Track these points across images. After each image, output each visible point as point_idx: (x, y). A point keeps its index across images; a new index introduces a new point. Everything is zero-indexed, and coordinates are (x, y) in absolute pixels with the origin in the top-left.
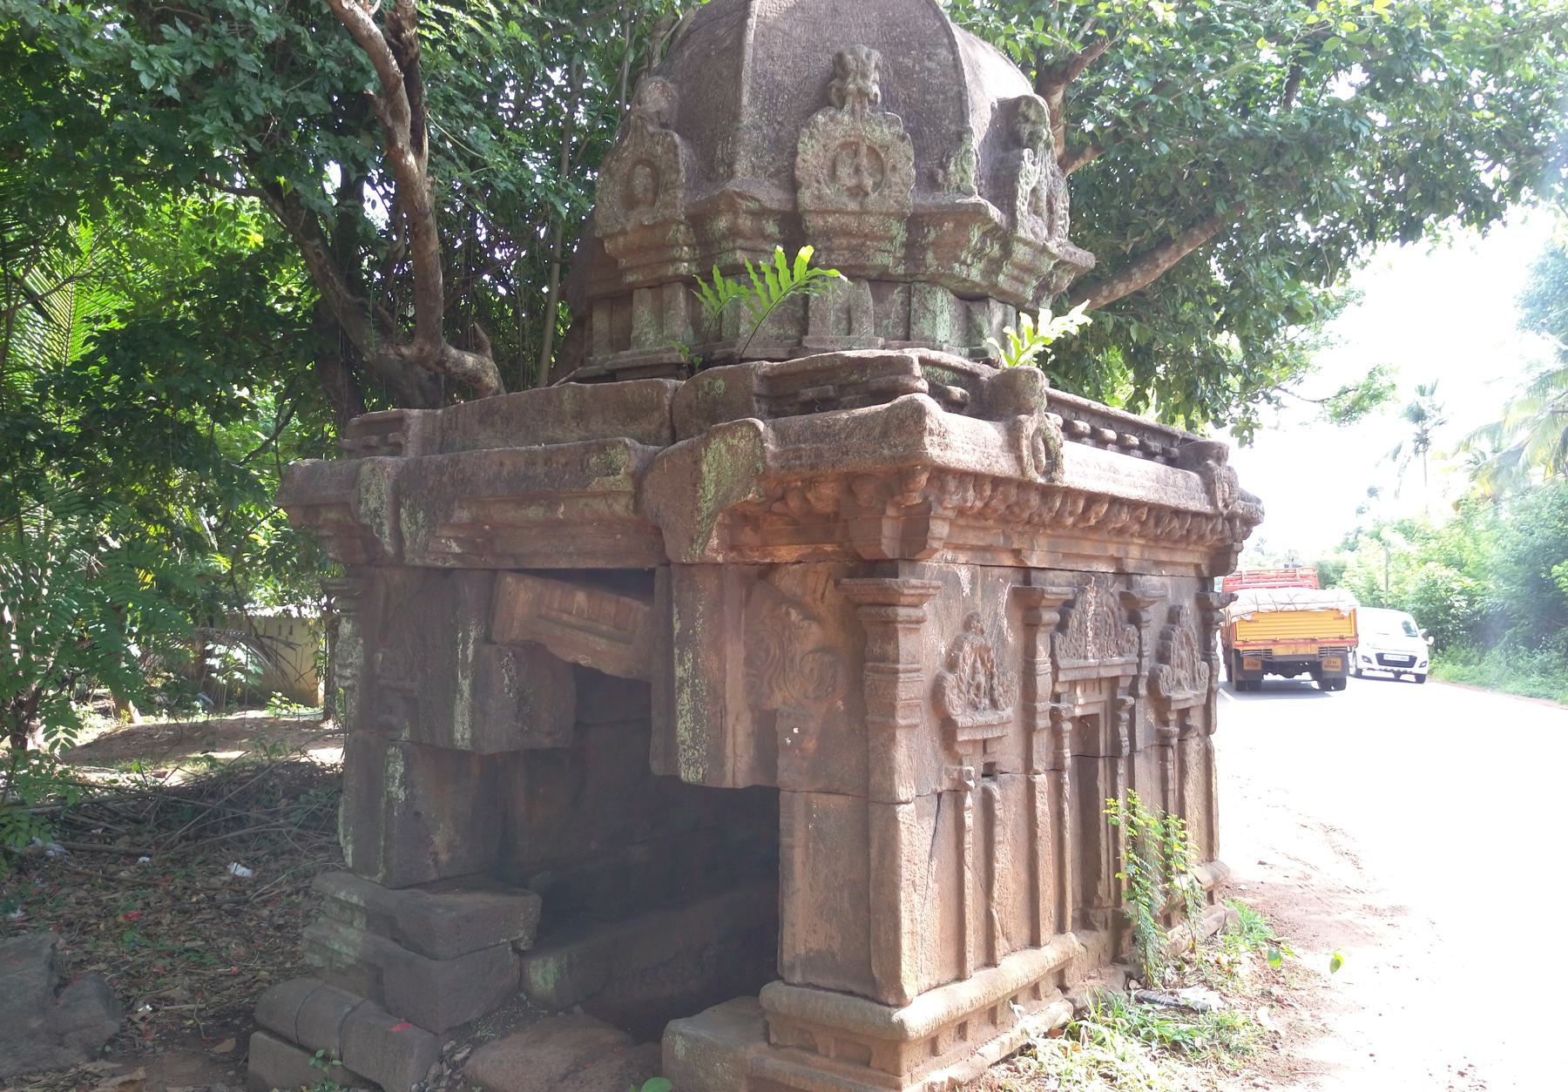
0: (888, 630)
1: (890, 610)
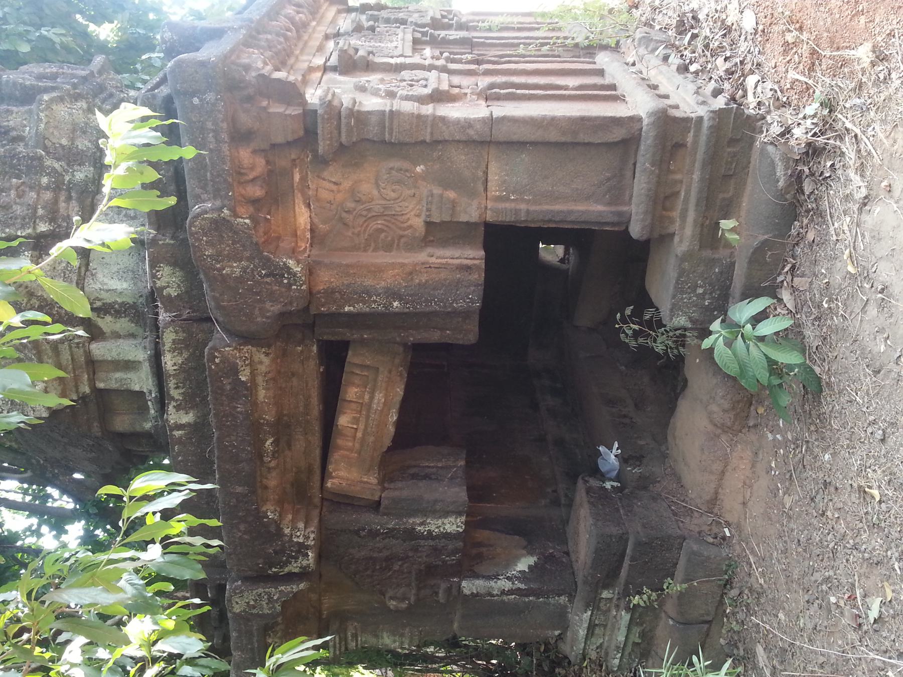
1: (343, 114)
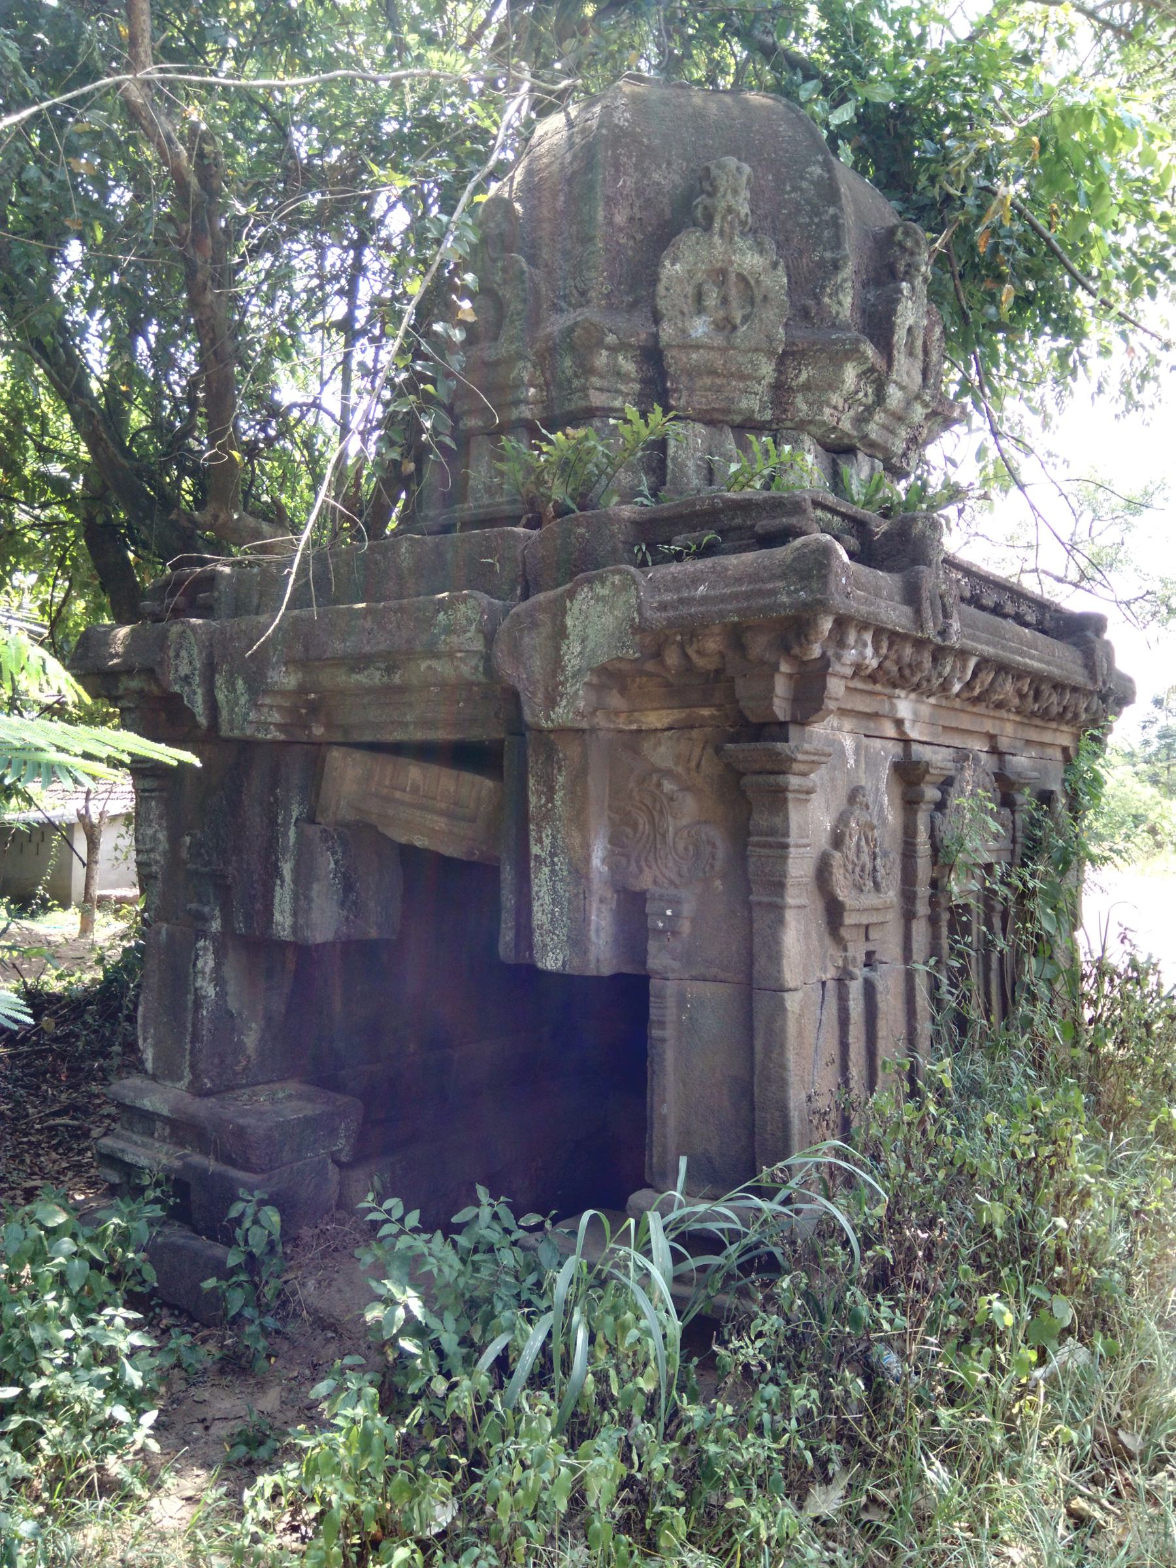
0: (778, 798)
1: (780, 779)
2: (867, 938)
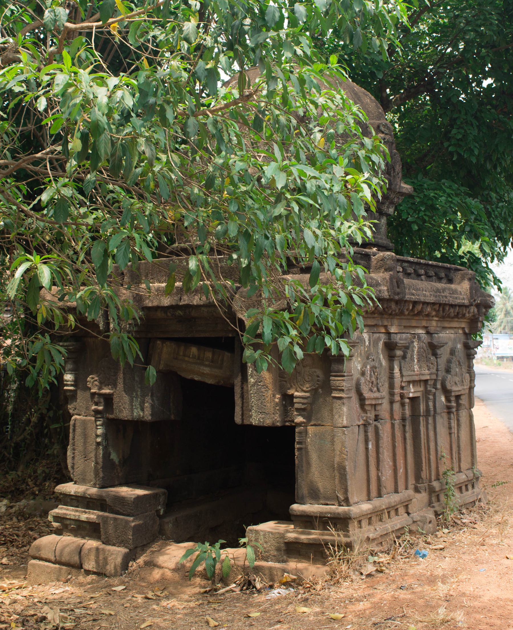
2: (375, 410)
